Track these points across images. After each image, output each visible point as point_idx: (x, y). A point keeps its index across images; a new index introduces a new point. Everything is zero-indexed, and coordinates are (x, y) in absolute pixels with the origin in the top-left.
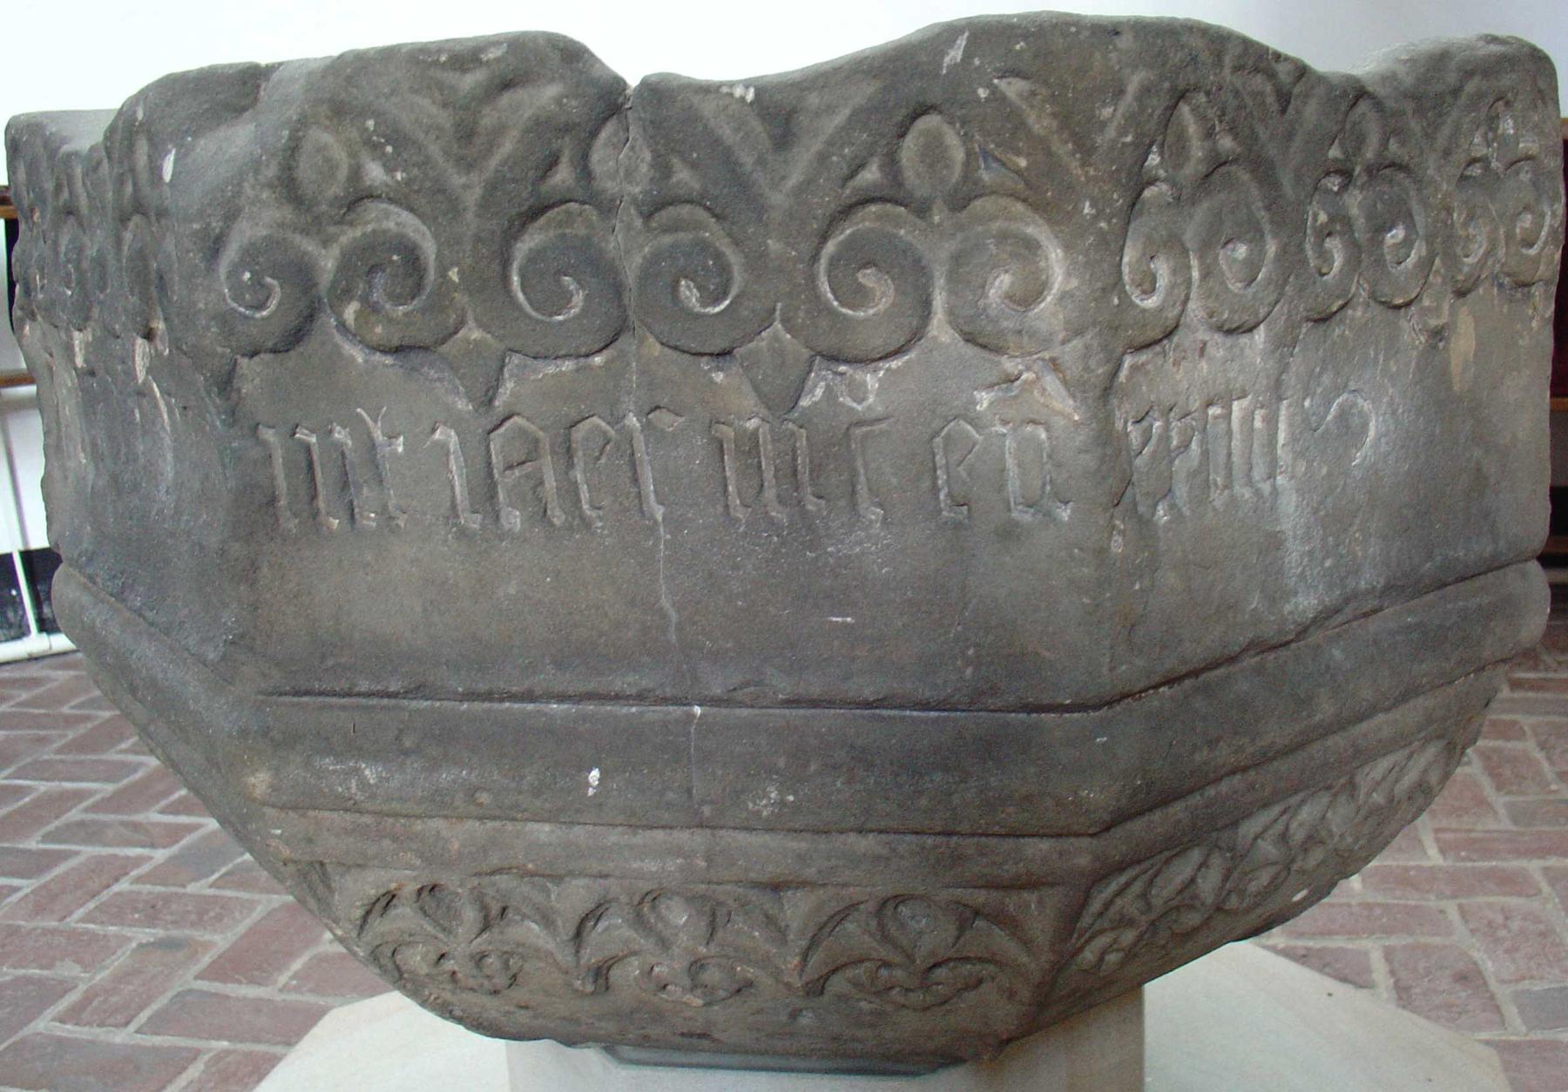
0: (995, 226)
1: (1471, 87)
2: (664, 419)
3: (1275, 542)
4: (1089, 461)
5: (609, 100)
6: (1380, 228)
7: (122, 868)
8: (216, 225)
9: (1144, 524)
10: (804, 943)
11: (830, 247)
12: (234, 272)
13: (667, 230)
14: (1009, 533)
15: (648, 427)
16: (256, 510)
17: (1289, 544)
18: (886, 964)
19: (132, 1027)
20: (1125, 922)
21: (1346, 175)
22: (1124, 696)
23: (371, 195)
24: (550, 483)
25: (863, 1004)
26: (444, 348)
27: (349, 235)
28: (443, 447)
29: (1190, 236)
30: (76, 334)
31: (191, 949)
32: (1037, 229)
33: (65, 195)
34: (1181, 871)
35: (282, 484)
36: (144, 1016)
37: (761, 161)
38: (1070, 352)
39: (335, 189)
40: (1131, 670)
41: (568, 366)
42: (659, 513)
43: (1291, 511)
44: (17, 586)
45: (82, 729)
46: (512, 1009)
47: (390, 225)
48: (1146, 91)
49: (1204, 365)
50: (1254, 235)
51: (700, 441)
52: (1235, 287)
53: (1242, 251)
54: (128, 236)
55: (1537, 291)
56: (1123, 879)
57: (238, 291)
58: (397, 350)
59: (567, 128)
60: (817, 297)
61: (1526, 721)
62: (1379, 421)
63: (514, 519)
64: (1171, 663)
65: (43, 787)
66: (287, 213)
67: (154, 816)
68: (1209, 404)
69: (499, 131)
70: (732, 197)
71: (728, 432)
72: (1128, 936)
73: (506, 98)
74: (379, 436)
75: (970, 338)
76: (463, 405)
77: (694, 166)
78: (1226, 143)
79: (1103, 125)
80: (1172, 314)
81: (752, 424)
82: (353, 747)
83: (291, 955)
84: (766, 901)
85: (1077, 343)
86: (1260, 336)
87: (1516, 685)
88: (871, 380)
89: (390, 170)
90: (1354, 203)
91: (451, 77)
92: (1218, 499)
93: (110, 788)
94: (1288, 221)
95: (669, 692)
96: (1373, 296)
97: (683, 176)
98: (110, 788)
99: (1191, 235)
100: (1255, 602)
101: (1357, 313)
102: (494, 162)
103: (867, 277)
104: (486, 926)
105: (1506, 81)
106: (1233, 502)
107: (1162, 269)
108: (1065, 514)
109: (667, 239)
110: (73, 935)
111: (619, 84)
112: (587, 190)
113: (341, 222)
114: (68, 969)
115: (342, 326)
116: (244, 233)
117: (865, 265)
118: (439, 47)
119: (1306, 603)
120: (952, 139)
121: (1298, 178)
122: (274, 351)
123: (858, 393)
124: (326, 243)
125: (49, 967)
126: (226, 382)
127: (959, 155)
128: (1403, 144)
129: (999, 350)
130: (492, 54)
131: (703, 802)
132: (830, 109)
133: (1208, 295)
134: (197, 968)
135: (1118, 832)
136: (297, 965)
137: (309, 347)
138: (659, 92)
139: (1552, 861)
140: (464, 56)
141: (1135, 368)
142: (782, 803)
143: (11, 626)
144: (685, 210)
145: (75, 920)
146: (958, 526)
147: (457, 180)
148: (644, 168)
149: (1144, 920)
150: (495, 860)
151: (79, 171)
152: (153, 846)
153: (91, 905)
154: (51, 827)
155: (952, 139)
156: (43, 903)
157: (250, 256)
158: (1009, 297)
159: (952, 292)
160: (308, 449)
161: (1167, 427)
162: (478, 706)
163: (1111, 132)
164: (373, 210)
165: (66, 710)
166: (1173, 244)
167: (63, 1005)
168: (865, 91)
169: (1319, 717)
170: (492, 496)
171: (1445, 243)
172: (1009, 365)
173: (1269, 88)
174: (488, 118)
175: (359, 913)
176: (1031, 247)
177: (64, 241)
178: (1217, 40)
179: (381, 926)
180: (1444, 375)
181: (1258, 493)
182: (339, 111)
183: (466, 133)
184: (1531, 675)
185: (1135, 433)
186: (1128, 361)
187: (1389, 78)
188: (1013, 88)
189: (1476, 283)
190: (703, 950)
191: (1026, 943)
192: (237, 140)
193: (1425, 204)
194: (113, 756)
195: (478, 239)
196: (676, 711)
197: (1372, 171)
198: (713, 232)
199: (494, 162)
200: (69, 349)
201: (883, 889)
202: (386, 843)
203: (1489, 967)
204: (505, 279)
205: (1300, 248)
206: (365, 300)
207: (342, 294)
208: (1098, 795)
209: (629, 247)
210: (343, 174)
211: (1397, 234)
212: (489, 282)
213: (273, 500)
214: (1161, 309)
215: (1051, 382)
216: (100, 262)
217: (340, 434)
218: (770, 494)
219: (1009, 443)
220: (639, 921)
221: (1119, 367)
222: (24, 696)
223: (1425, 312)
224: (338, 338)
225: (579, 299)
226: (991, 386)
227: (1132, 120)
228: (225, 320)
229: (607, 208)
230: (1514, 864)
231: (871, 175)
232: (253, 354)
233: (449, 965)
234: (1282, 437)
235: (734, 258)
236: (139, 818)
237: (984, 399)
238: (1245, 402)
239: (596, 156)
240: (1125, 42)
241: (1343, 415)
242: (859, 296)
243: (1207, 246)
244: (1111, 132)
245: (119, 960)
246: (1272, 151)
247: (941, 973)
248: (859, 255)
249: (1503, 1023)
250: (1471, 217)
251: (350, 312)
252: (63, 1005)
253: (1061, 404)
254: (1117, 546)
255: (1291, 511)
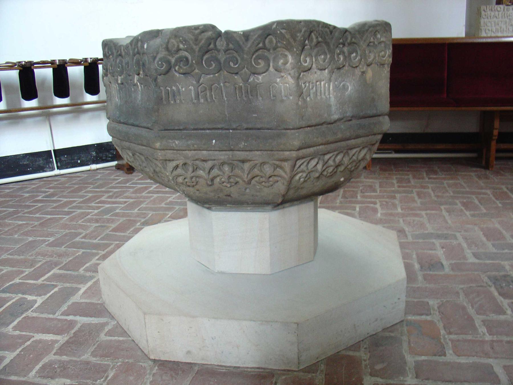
0: (280, 53)
1: (370, 29)
2: (227, 84)
3: (329, 106)
4: (295, 89)
5: (219, 34)
6: (350, 53)
7: (88, 214)
8: (155, 55)
9: (305, 101)
10: (247, 172)
11: (254, 56)
12: (158, 62)
13: (228, 54)
14: (282, 101)
15: (224, 85)
16: (159, 101)
17: (333, 106)
18: (262, 177)
19: (97, 240)
20: (302, 171)
21: (344, 45)
22: (301, 128)
23: (181, 50)
24: (208, 94)
25: (258, 187)
26: (192, 73)
27: (177, 56)
28: (191, 90)
29: (313, 54)
30: (119, 77)
31: (108, 227)
32: (287, 53)
33: (119, 52)
34: (313, 163)
35: (164, 96)
36: (99, 238)
37: (243, 43)
38: (292, 72)
39: (175, 49)
40: (303, 123)
41: (212, 76)
42: (226, 99)
43: (333, 100)
44: (52, 158)
45: (72, 189)
46: (196, 191)
47: (183, 54)
48: (305, 31)
49: (316, 75)
50: (325, 54)
51: (232, 87)
52: (321, 62)
53: (323, 57)
54: (135, 58)
55: (386, 66)
56: (302, 161)
57: (158, 65)
58: (184, 74)
59: (213, 38)
60: (252, 64)
61: (430, 185)
62: (351, 87)
63: (202, 101)
64: (309, 123)
65: (65, 200)
66: (167, 53)
67: (93, 204)
68: (317, 82)
69: (202, 39)
70: (239, 49)
71: (237, 86)
72: (304, 175)
73: (203, 34)
74: (180, 88)
75: (276, 70)
76: (194, 82)
77: (233, 44)
78: (320, 39)
79: (298, 37)
80: (310, 66)
81: (241, 84)
82: (174, 138)
83: (130, 228)
84: (240, 164)
85: (293, 71)
86: (326, 71)
87: (429, 178)
88: (260, 77)
89: (184, 46)
90: (346, 49)
91: (194, 31)
92: (319, 98)
93: (82, 200)
94: (332, 53)
95: (226, 127)
96: (349, 65)
97: (231, 46)
98: (82, 200)
99: (313, 54)
100: (326, 115)
101: (346, 68)
102: (201, 44)
103: (260, 61)
104: (193, 172)
105: (378, 28)
106: (322, 98)
107: (308, 59)
108: (291, 98)
109: (228, 56)
110: (80, 225)
111: (221, 32)
112: (216, 48)
113: (176, 54)
114: (80, 231)
115: (175, 70)
116: (159, 56)
117: (260, 59)
118: (192, 26)
119: (336, 117)
120: (274, 40)
121: (334, 45)
122: (164, 74)
123: (258, 79)
124: (173, 57)
125: (77, 230)
126: (156, 80)
127: (275, 42)
128: (355, 39)
129: (281, 72)
130: (201, 27)
131: (232, 145)
132: (255, 35)
133: (316, 63)
134: (109, 230)
135: (301, 151)
136: (131, 229)
137: (169, 74)
138: (227, 33)
139: (428, 212)
140: (196, 28)
141: (303, 75)
142: (245, 145)
143: (50, 168)
144: (231, 51)
145: (80, 222)
146: (274, 100)
147: (194, 47)
148: (225, 45)
149: (307, 171)
150: (197, 157)
151: (122, 48)
152: (94, 210)
153: (83, 220)
154: (70, 206)
155: (274, 40)
156: (72, 219)
157: (161, 59)
158: (282, 64)
159: (273, 63)
160: (168, 90)
161: (309, 85)
162: (195, 131)
163: (299, 38)
164: (181, 52)
165: (67, 185)
166: (310, 56)
167: (81, 236)
168: (260, 32)
169: (338, 137)
170: (199, 97)
171: (364, 56)
172: (282, 74)
173: (328, 30)
174: (200, 37)
175: (172, 170)
176: (286, 56)
177: (118, 61)
178: (319, 23)
179: (175, 173)
180: (365, 81)
181: (326, 97)
182: (176, 36)
183: (196, 40)
184: (435, 176)
185: (303, 86)
186: (302, 74)
187: (353, 28)
188: (283, 31)
189: (371, 64)
190: (230, 174)
191: (285, 172)
192: (158, 41)
193: (360, 50)
194: (80, 194)
195: (198, 56)
196: (227, 131)
197: (349, 44)
198: (235, 54)
199: (201, 44)
200: (117, 80)
201: (261, 161)
202: (178, 155)
203: (406, 229)
204: (202, 63)
205: (334, 56)
206: (179, 66)
207: (175, 65)
208: (296, 143)
209: (222, 57)
210: (176, 46)
211: (354, 54)
212: (199, 63)
213: (162, 99)
214: (307, 66)
215: (289, 77)
216: (127, 64)
217: (174, 88)
218: (244, 96)
219: (282, 87)
220: (220, 169)
221: (300, 74)
222: (56, 183)
223: (360, 68)
224: (174, 72)
225: (214, 65)
226: (279, 78)
227: (303, 36)
228: (156, 70)
229: (219, 51)
230: (418, 212)
231: (261, 45)
232: (160, 75)
233: (186, 180)
234: (331, 88)
235: (239, 59)
236: (90, 205)
237: (278, 80)
238: (324, 82)
239: (217, 43)
240: (302, 23)
241: (344, 85)
242: (258, 64)
243: (316, 56)
244: (299, 38)
245: (91, 229)
246: (329, 41)
247: (271, 179)
248: (259, 57)
249: (407, 239)
250: (370, 52)
251: (177, 68)
252: (81, 236)
253: (291, 80)
254: (300, 103)
255: (333, 100)
